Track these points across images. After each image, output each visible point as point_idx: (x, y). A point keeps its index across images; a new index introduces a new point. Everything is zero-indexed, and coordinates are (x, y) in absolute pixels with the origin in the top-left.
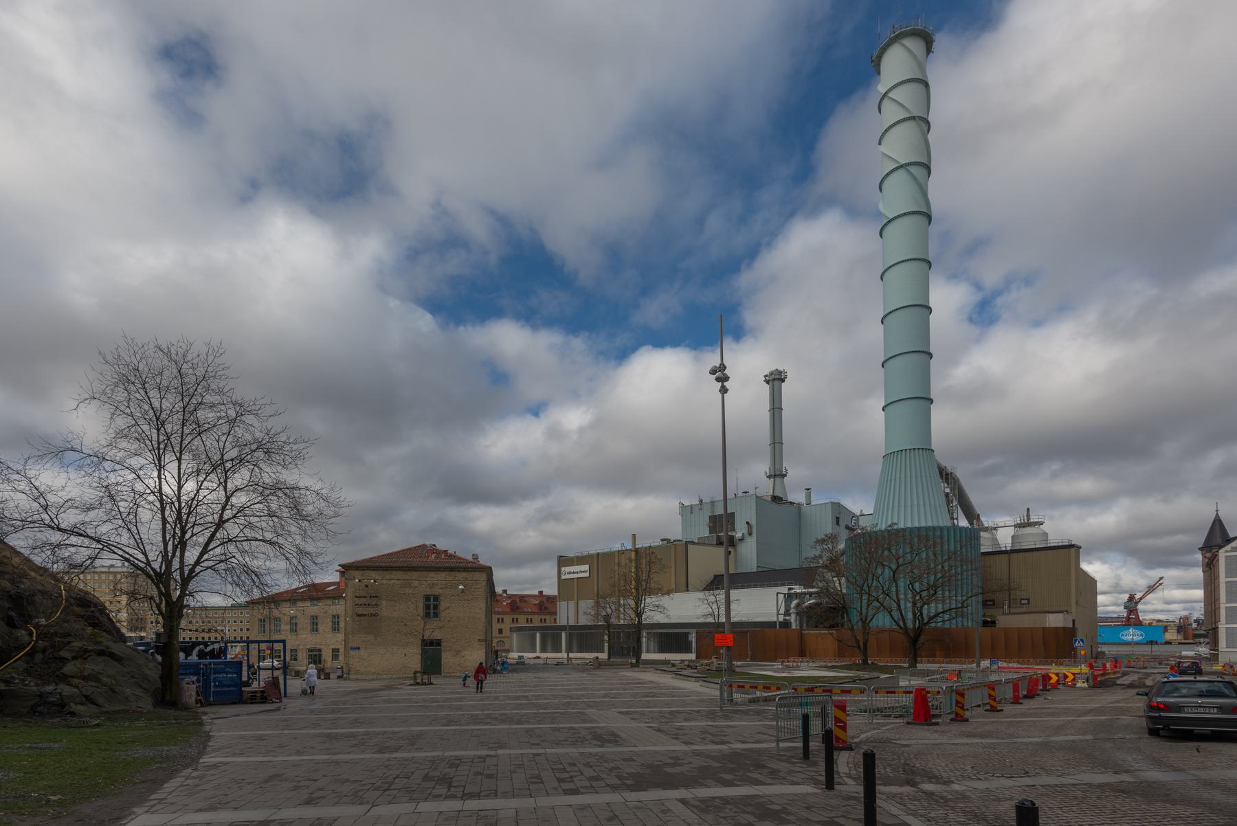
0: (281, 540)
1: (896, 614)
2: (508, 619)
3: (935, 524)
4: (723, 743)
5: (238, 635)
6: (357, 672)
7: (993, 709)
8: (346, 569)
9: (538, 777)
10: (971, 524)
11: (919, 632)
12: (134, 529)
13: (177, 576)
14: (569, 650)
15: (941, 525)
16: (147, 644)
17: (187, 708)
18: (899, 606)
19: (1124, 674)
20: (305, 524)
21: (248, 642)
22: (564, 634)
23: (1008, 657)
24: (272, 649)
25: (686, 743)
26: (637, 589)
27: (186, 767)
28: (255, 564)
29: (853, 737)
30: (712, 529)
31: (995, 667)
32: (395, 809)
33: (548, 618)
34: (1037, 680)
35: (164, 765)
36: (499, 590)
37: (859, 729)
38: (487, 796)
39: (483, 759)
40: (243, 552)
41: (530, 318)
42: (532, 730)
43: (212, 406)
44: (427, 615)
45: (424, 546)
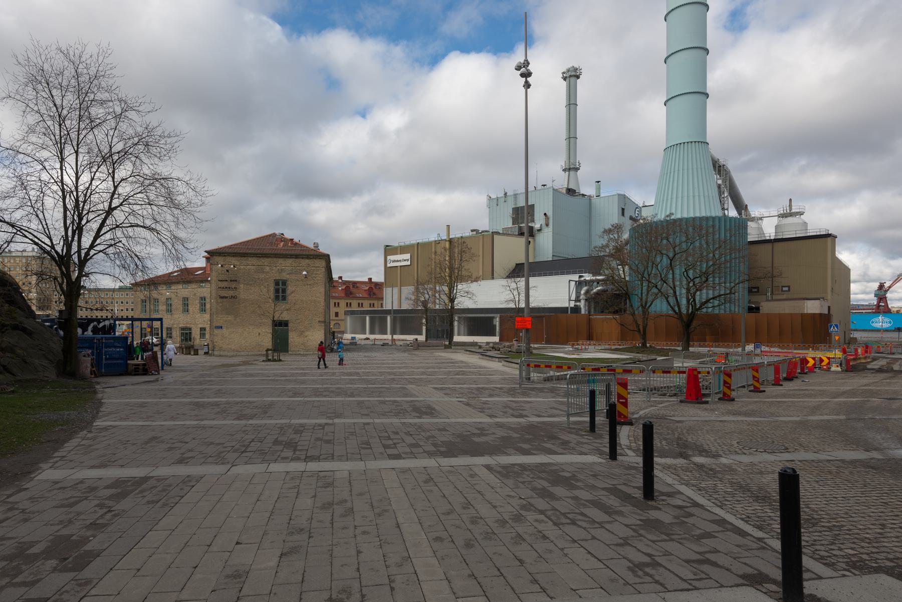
0: (159, 227)
1: (672, 300)
2: (343, 303)
3: (708, 215)
4: (521, 416)
5: (125, 314)
6: (221, 349)
7: (756, 390)
8: (212, 255)
9: (368, 443)
10: (740, 214)
11: (692, 317)
12: (41, 216)
13: (75, 258)
14: (393, 332)
15: (713, 215)
16: (52, 321)
17: (83, 378)
18: (675, 292)
19: (874, 359)
20: (176, 212)
21: (133, 319)
22: (389, 318)
23: (770, 342)
24: (152, 328)
25: (491, 416)
26: (450, 277)
27: (82, 430)
28: (137, 249)
29: (633, 413)
30: (515, 221)
31: (758, 351)
32: (251, 469)
33: (376, 302)
34: (796, 364)
35: (64, 427)
36: (335, 276)
37: (639, 406)
38: (326, 459)
39: (323, 426)
40: (128, 237)
41: (360, 29)
42: (362, 402)
43: (102, 103)
44: (277, 298)
45: (274, 235)
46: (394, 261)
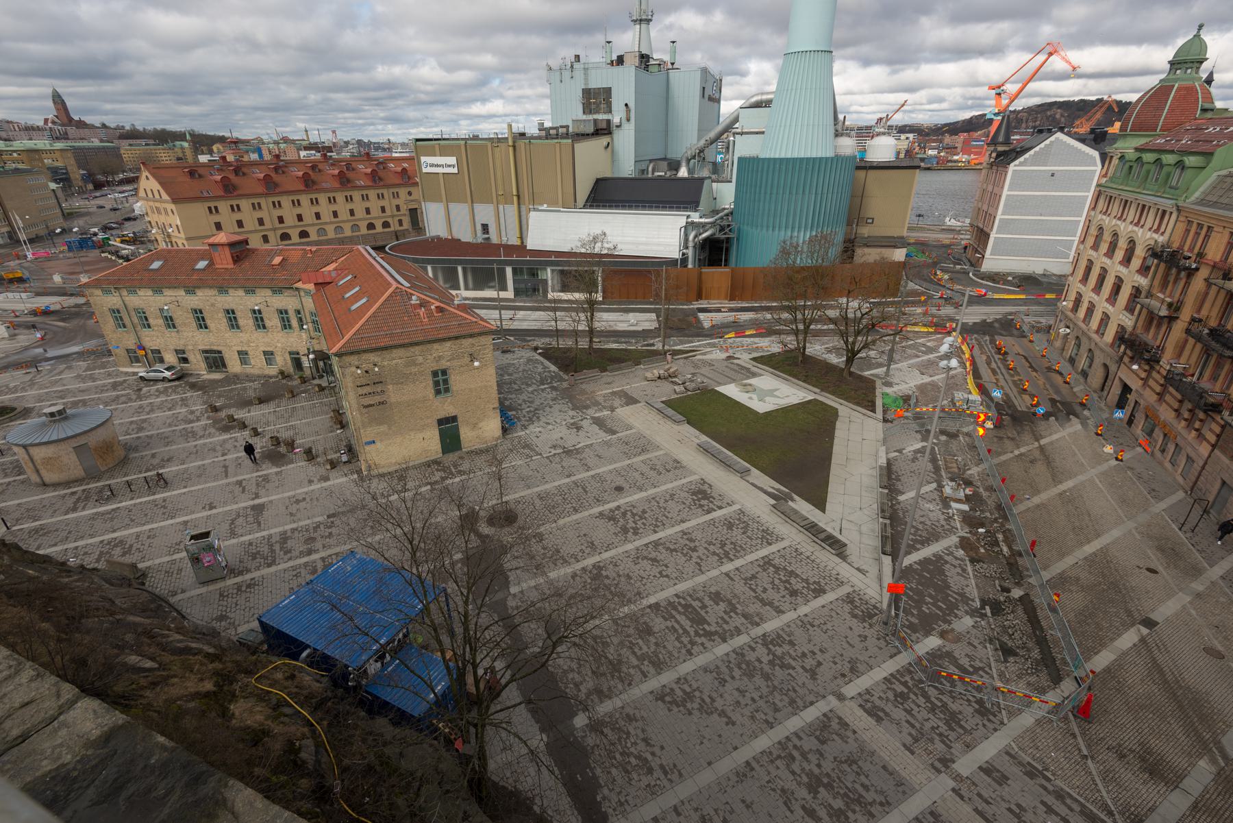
46: (432, 165)
